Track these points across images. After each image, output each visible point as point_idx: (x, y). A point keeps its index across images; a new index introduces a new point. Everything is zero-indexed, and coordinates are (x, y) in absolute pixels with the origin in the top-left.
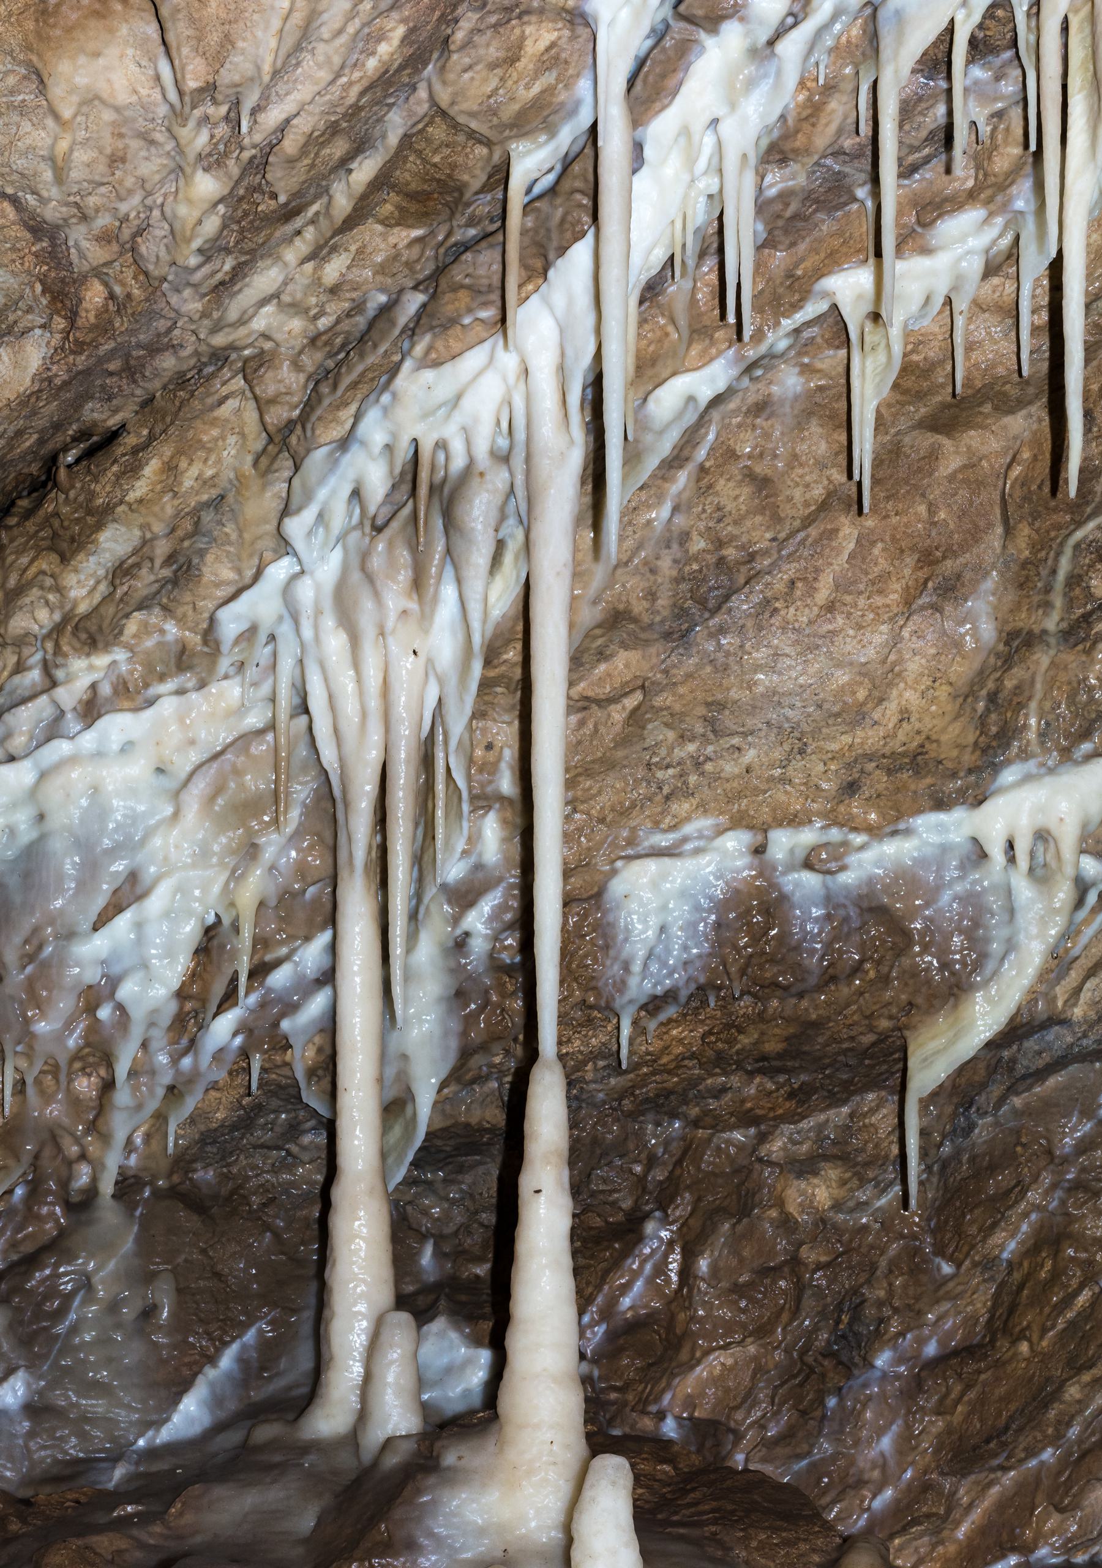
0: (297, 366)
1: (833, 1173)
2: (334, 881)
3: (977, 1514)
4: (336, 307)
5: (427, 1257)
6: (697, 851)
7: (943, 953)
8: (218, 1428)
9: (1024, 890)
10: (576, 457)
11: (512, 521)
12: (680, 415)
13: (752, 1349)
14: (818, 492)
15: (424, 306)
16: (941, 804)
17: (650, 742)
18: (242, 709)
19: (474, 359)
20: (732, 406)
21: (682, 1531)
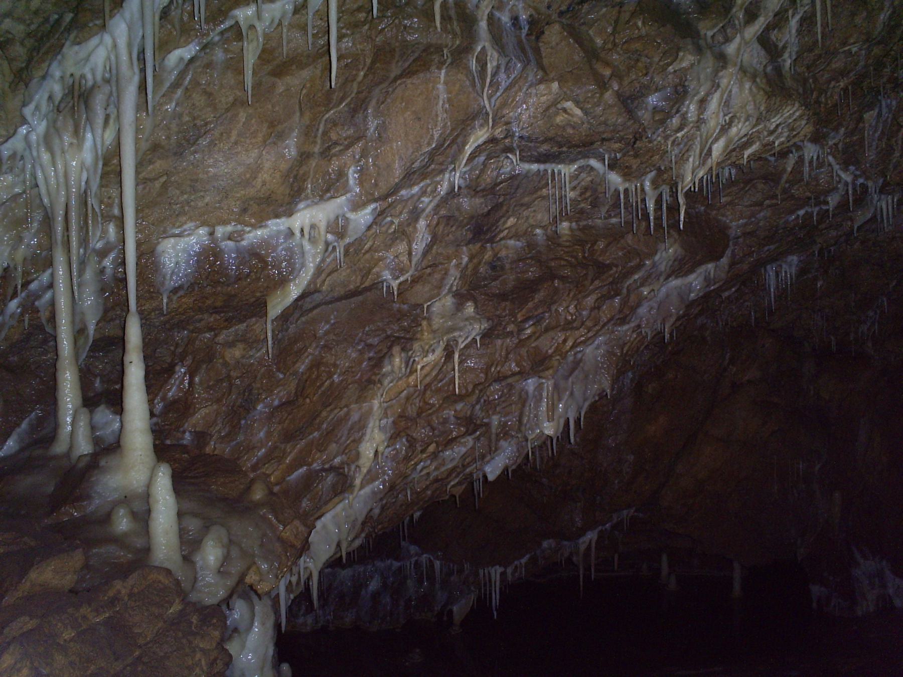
0: (22, 43)
1: (241, 346)
2: (51, 249)
3: (292, 455)
4: (38, 21)
5: (97, 384)
6: (189, 235)
7: (279, 268)
8: (22, 450)
9: (307, 247)
10: (136, 79)
11: (112, 106)
12: (177, 66)
13: (215, 407)
14: (231, 99)
15: (73, 19)
16: (277, 216)
17: (170, 195)
18: (14, 185)
19: (94, 41)
20: (198, 64)
21: (193, 481)
